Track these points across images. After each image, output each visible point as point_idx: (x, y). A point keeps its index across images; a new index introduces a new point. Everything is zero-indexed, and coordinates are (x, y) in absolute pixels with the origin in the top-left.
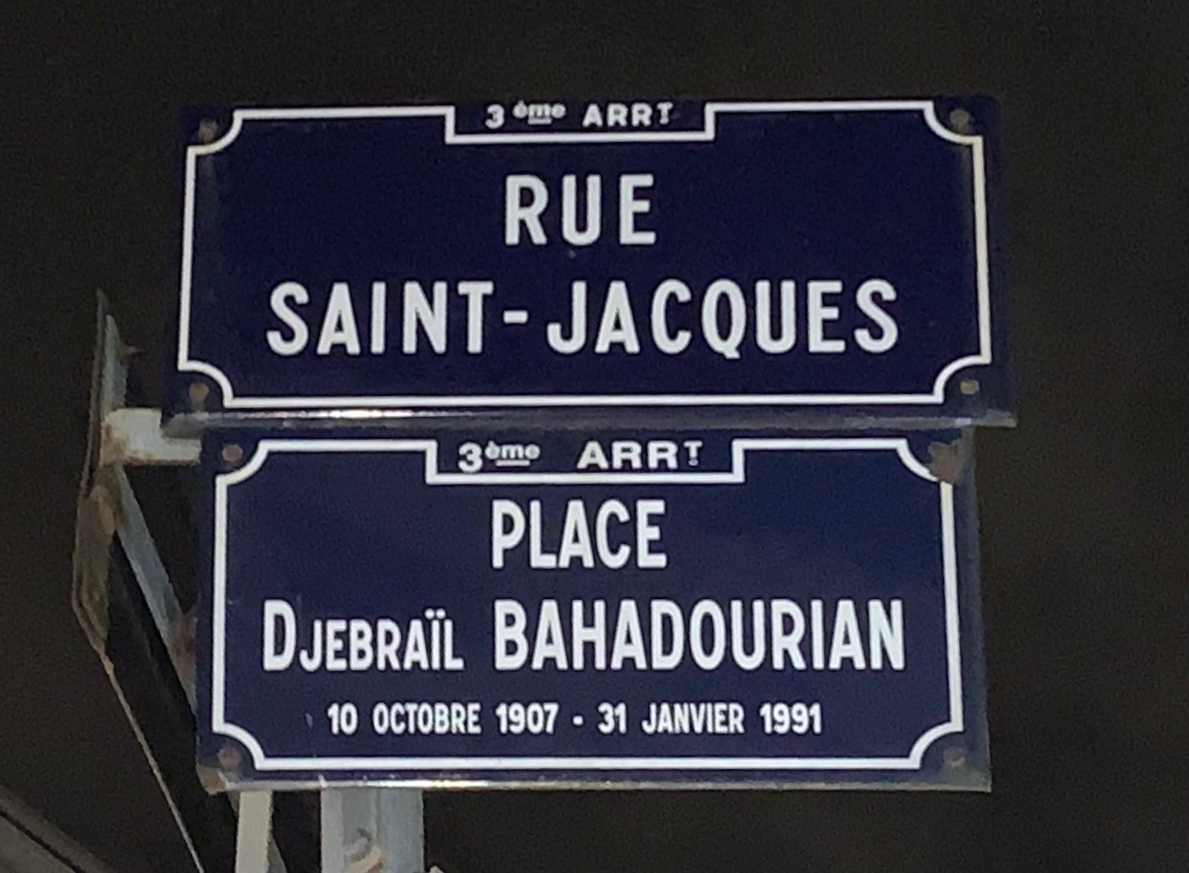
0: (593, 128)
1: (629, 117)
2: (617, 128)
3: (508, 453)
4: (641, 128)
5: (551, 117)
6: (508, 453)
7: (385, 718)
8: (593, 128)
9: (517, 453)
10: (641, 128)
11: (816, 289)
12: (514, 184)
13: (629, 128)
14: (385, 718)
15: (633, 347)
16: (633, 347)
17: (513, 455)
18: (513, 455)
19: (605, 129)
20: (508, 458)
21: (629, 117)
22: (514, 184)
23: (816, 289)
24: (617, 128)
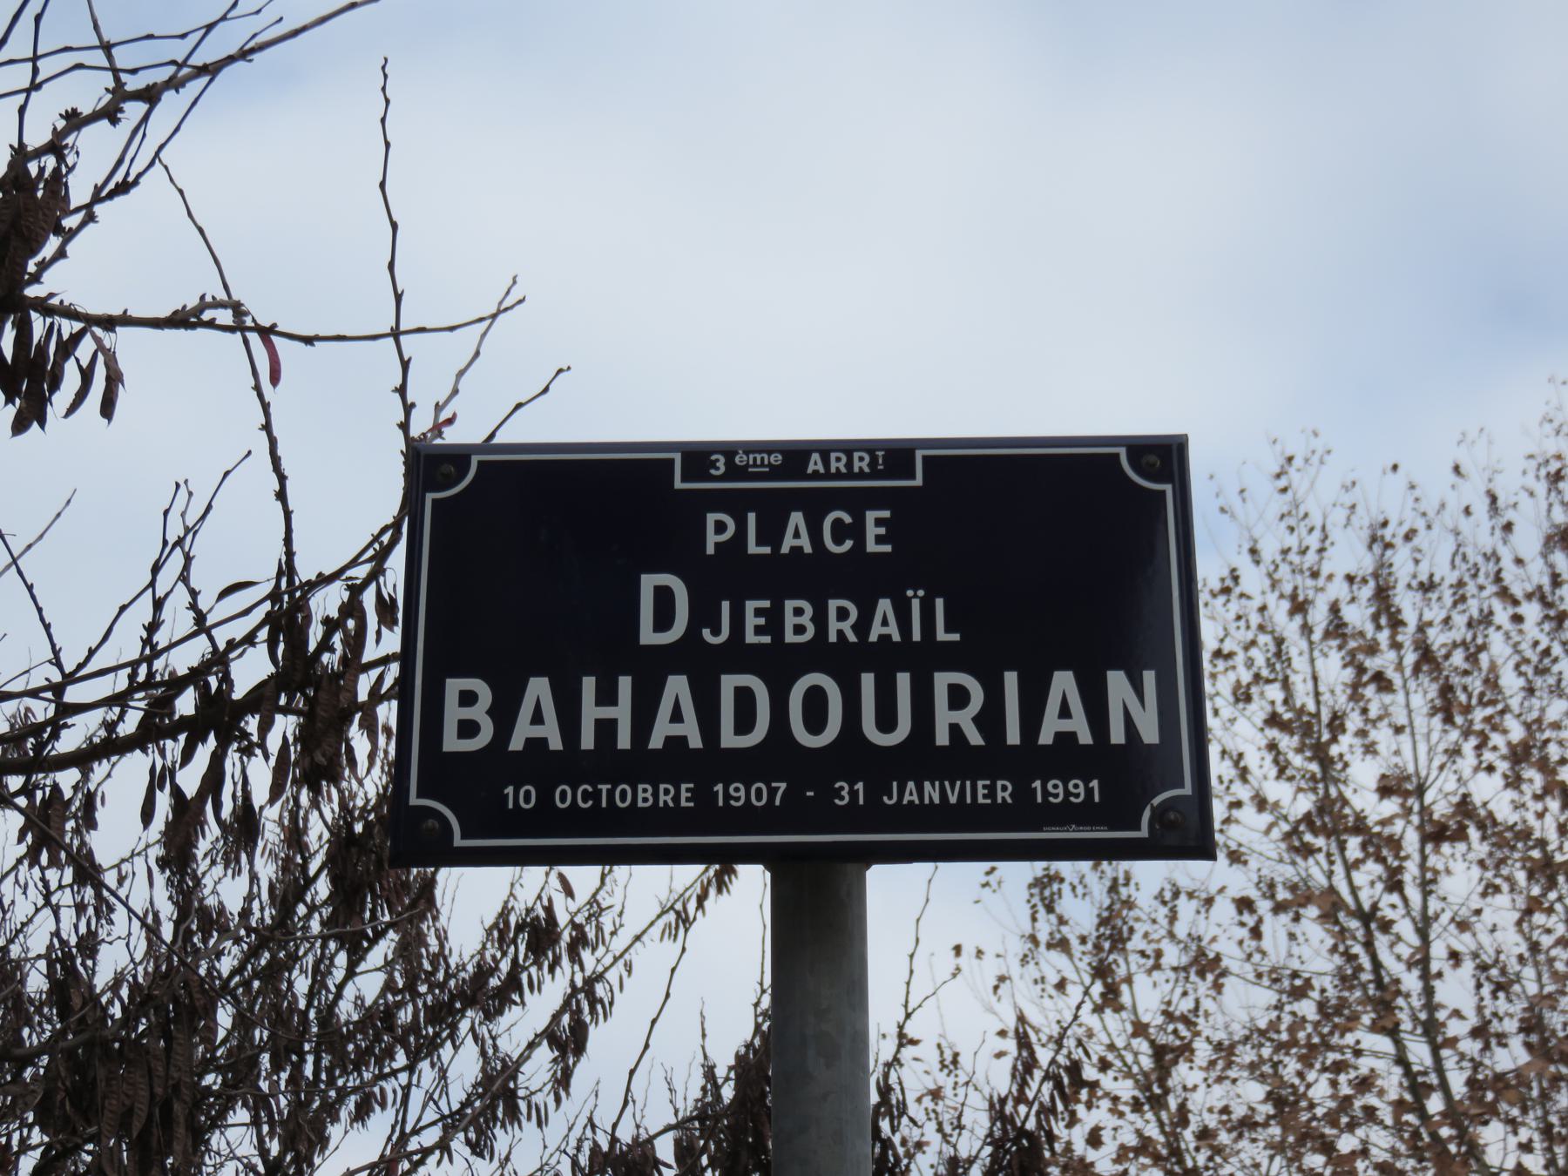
0: (816, 476)
1: (849, 464)
2: (838, 476)
3: (755, 459)
4: (861, 475)
5: (770, 465)
6: (755, 459)
7: (565, 796)
8: (816, 476)
9: (762, 459)
10: (861, 475)
11: (980, 783)
12: (711, 518)
13: (850, 475)
14: (565, 796)
15: (808, 549)
16: (808, 549)
17: (759, 462)
18: (759, 462)
19: (828, 476)
20: (755, 465)
21: (849, 464)
22: (711, 518)
23: (980, 783)
24: (838, 476)
